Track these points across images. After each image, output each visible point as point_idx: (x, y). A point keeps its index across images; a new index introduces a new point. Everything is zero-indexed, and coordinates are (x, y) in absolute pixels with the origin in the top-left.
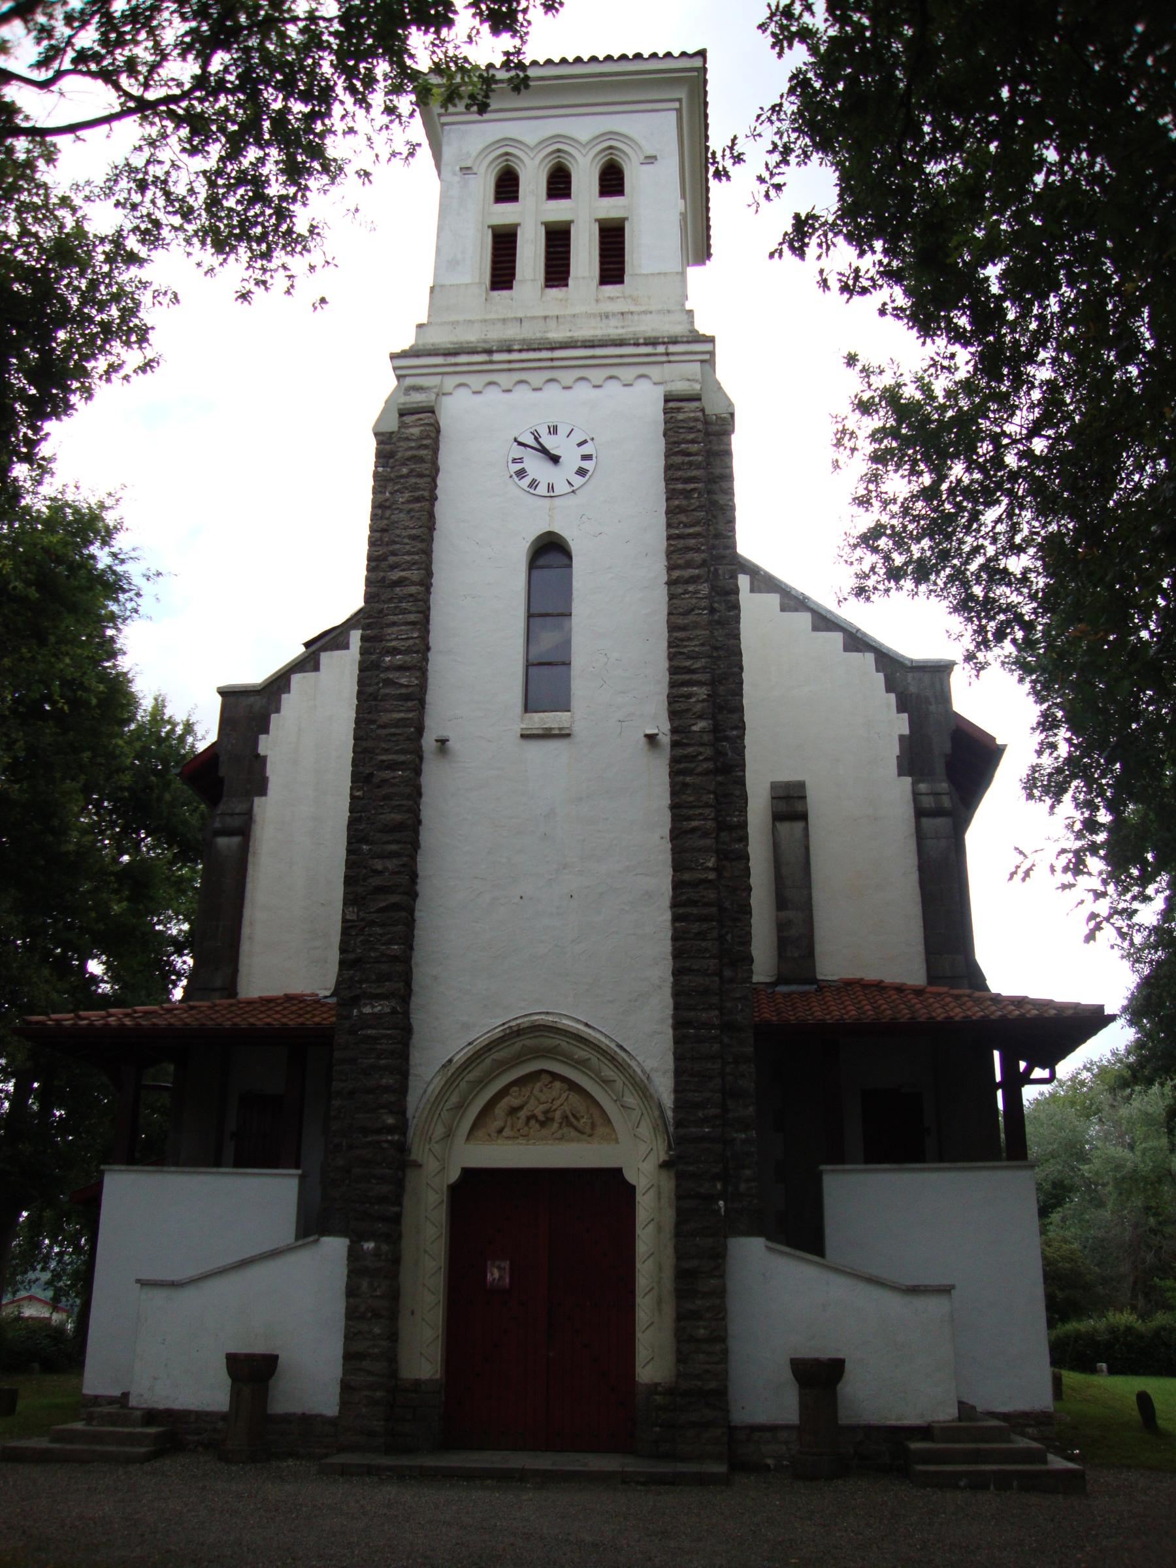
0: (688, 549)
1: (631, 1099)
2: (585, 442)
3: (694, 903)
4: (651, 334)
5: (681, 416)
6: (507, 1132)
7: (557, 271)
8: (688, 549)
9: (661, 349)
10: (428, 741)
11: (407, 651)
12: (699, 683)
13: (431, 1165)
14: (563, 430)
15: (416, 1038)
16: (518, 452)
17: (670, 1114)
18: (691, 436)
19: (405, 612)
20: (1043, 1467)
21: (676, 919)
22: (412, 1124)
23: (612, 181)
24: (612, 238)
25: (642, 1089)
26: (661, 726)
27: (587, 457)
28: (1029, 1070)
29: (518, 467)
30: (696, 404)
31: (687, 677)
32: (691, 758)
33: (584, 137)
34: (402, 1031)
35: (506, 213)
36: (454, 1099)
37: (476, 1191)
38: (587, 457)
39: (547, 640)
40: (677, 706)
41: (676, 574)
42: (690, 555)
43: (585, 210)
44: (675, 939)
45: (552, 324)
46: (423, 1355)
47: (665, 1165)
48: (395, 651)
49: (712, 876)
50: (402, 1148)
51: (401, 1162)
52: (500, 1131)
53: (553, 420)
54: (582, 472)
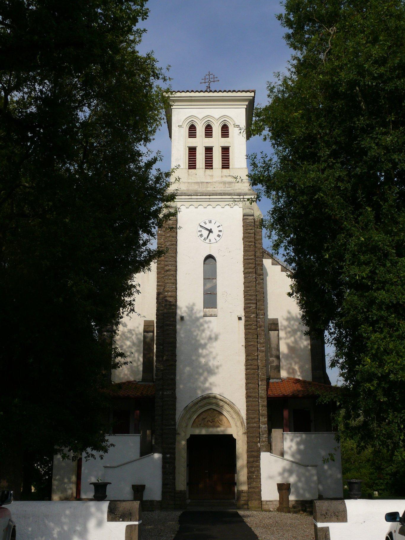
0: (250, 263)
1: (235, 416)
2: (219, 226)
3: (251, 365)
4: (238, 191)
5: (248, 221)
6: (202, 425)
7: (209, 165)
8: (250, 263)
9: (242, 197)
10: (178, 317)
11: (172, 291)
12: (253, 303)
13: (183, 434)
14: (213, 222)
15: (178, 400)
16: (200, 229)
17: (245, 421)
18: (251, 228)
19: (170, 279)
20: (187, 493)
21: (246, 369)
22: (177, 424)
23: (225, 131)
24: (225, 150)
25: (238, 414)
26: (242, 314)
27: (220, 231)
28: (353, 384)
29: (200, 233)
30: (252, 217)
31: (250, 301)
32: (250, 325)
33: (217, 117)
34: (173, 398)
35: (192, 142)
36: (188, 416)
37: (195, 441)
38: (220, 231)
39: (209, 286)
40: (247, 310)
41: (247, 271)
42: (250, 265)
43: (217, 142)
44: (246, 374)
45: (209, 185)
46: (181, 483)
47: (245, 433)
48: (168, 291)
49: (256, 358)
50: (175, 430)
51: (174, 433)
52: (200, 424)
53: (210, 218)
54: (219, 236)
